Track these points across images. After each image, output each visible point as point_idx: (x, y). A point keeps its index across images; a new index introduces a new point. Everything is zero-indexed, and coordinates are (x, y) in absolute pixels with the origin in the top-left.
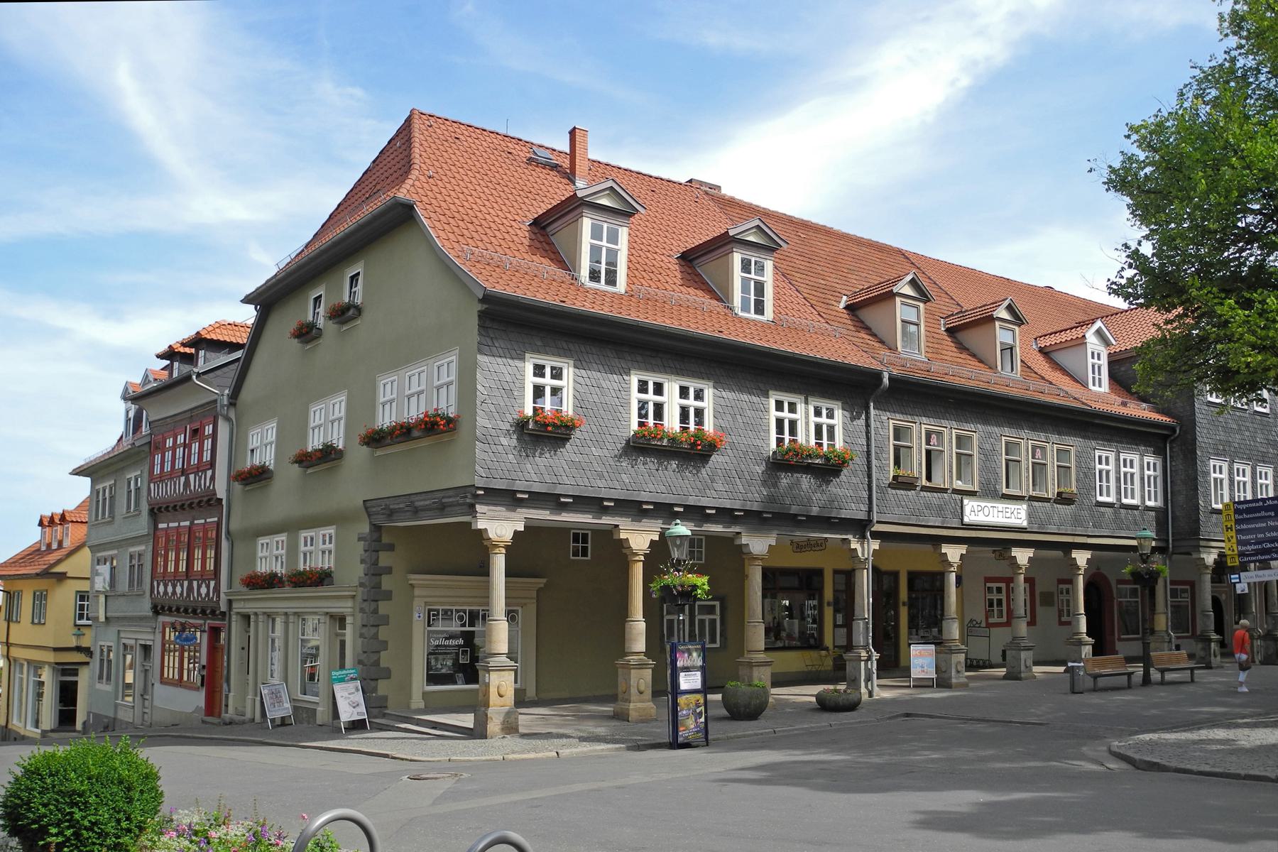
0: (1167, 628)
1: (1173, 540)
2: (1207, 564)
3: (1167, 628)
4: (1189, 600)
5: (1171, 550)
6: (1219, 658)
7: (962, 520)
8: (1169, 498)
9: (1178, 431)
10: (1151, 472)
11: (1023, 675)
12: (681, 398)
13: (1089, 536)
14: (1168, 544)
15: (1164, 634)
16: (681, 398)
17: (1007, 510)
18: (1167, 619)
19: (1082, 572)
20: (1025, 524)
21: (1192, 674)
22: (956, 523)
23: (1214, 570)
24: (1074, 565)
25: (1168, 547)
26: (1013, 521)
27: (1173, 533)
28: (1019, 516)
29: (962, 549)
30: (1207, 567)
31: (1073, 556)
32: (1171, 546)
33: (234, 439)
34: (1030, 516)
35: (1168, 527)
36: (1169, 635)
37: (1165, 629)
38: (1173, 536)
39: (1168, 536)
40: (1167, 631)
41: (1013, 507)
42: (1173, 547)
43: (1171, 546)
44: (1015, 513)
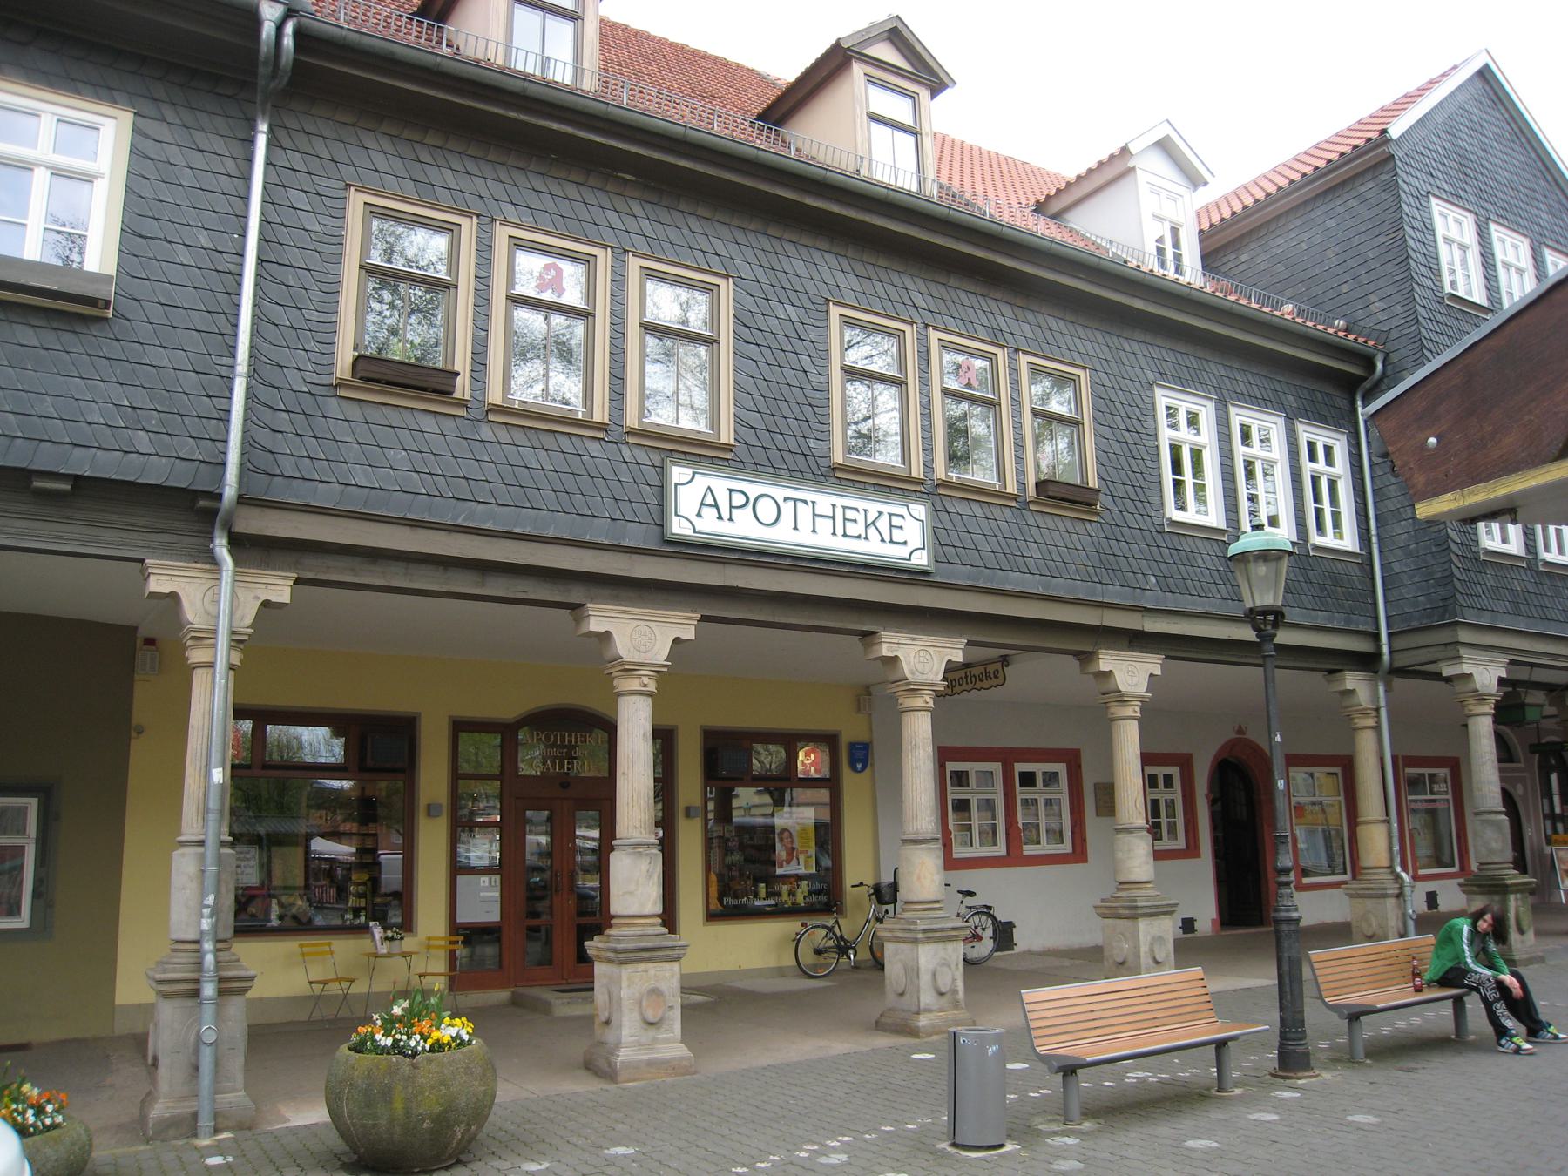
0: (1392, 859)
1: (1390, 635)
2: (1482, 690)
3: (1392, 859)
4: (1450, 797)
5: (1386, 657)
6: (1530, 935)
7: (661, 524)
8: (1373, 531)
9: (1379, 366)
10: (1321, 465)
11: (923, 1021)
12: (994, 800)
13: (1145, 610)
14: (1379, 647)
15: (1385, 876)
16: (994, 800)
17: (850, 514)
18: (1390, 838)
19: (1134, 710)
20: (921, 560)
21: (849, 520)
22: (635, 536)
23: (1499, 707)
24: (1106, 691)
25: (1377, 656)
26: (873, 548)
27: (1388, 617)
28: (898, 535)
29: (682, 625)
30: (1481, 699)
31: (1104, 666)
32: (1385, 649)
33: (642, 921)
34: (938, 538)
35: (1375, 604)
36: (1398, 877)
37: (1385, 863)
38: (1388, 627)
39: (1378, 626)
40: (1391, 867)
41: (874, 507)
42: (1391, 652)
43: (1385, 649)
44: (883, 524)
